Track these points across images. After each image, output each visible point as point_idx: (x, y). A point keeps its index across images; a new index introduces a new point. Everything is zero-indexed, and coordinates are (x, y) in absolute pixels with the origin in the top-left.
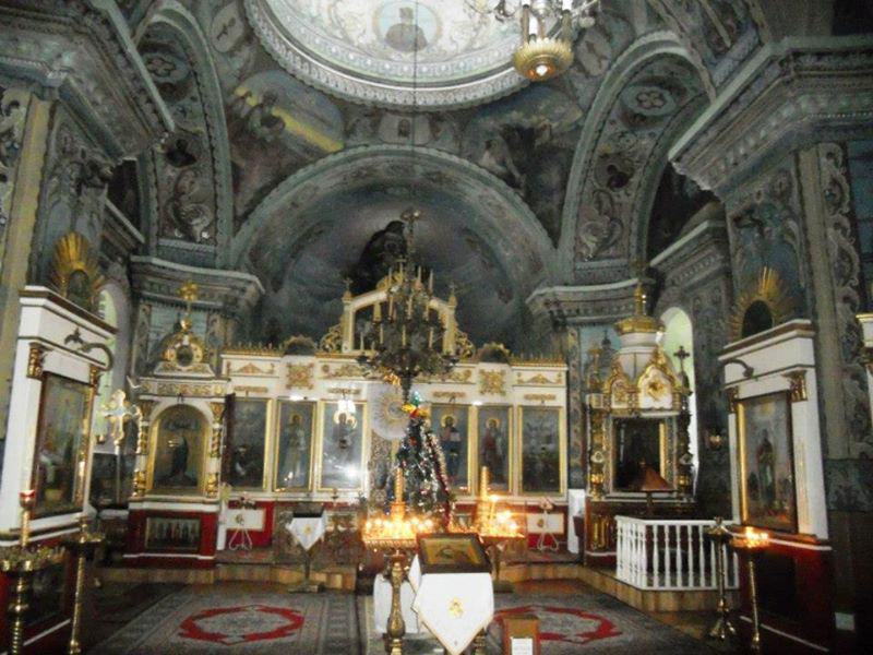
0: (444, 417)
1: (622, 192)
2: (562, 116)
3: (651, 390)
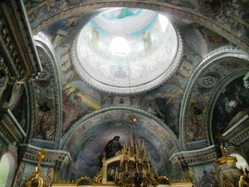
1: (200, 116)
2: (175, 93)
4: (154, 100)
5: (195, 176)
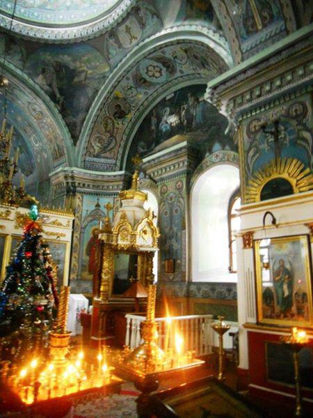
2: (96, 67)
4: (54, 64)
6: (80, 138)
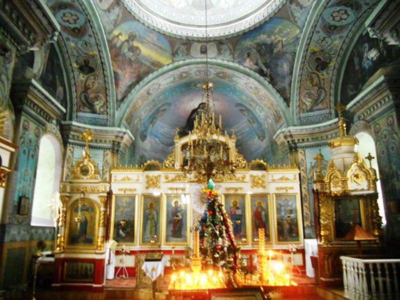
0: (232, 201)
1: (324, 73)
2: (288, 34)
3: (355, 178)
4: (255, 46)
5: (305, 161)
6: (291, 98)
